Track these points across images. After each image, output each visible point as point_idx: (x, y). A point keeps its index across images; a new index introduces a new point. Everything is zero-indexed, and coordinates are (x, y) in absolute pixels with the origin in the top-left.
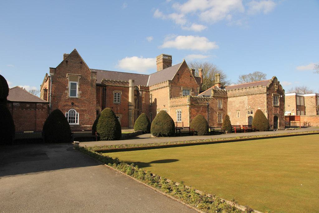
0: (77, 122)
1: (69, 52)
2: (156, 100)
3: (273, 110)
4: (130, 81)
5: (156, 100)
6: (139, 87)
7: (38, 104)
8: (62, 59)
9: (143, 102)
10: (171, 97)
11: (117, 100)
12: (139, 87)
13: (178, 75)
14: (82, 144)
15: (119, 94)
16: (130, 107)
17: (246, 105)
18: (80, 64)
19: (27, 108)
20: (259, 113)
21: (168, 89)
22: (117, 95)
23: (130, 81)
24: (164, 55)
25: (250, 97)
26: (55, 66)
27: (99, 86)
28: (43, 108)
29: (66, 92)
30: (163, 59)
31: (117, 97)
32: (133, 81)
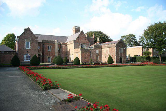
0: (29, 60)
1: (27, 28)
2: (70, 50)
3: (119, 55)
4: (56, 41)
5: (70, 50)
6: (61, 43)
7: (11, 52)
8: (24, 31)
9: (64, 50)
10: (74, 48)
11: (49, 49)
12: (61, 43)
13: (79, 37)
14: (32, 70)
15: (50, 47)
16: (56, 53)
17: (108, 52)
18: (31, 34)
19: (7, 54)
20: (35, 56)
21: (73, 44)
22: (49, 47)
23: (56, 41)
24: (76, 27)
25: (110, 48)
26: (20, 35)
27: (40, 43)
28: (13, 54)
29: (25, 46)
30: (76, 29)
31: (49, 48)
32: (57, 40)
